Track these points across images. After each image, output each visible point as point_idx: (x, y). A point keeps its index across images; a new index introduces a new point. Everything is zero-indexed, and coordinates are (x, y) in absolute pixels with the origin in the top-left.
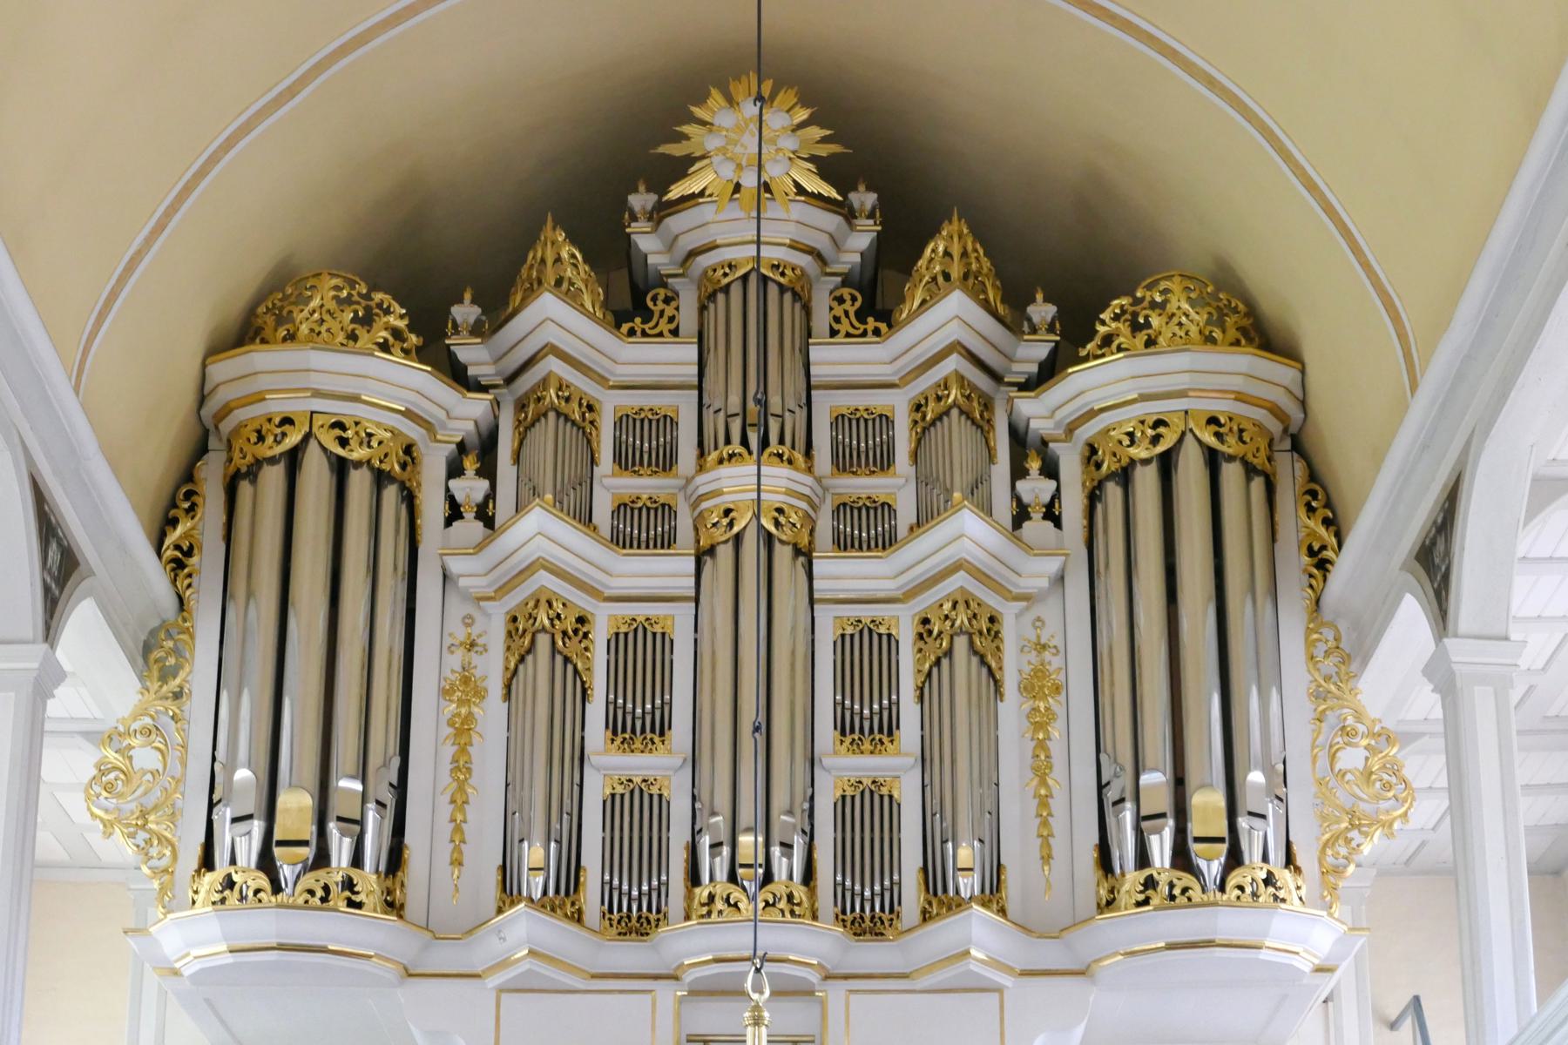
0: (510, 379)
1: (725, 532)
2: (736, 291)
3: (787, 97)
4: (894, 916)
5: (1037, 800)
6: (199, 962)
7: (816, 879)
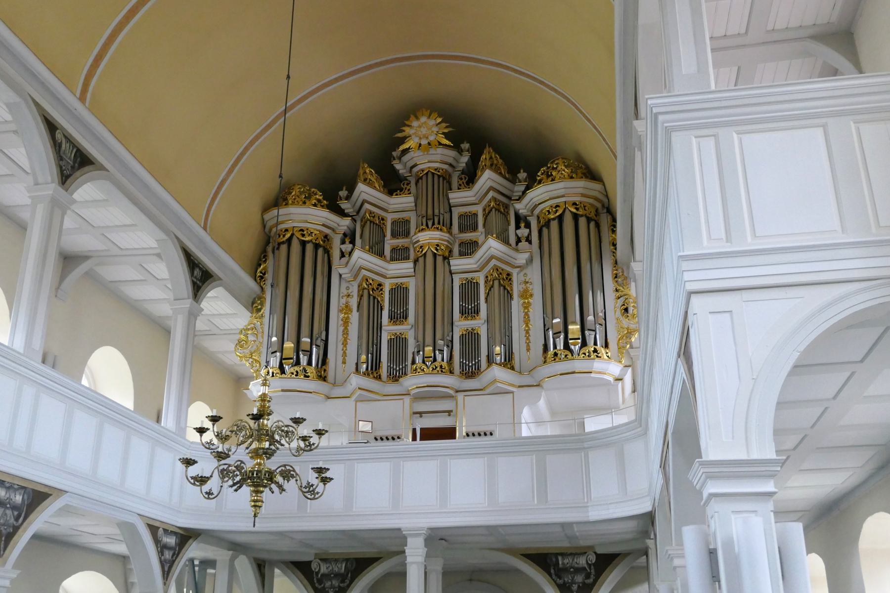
0: (358, 212)
2: (424, 178)
3: (435, 115)
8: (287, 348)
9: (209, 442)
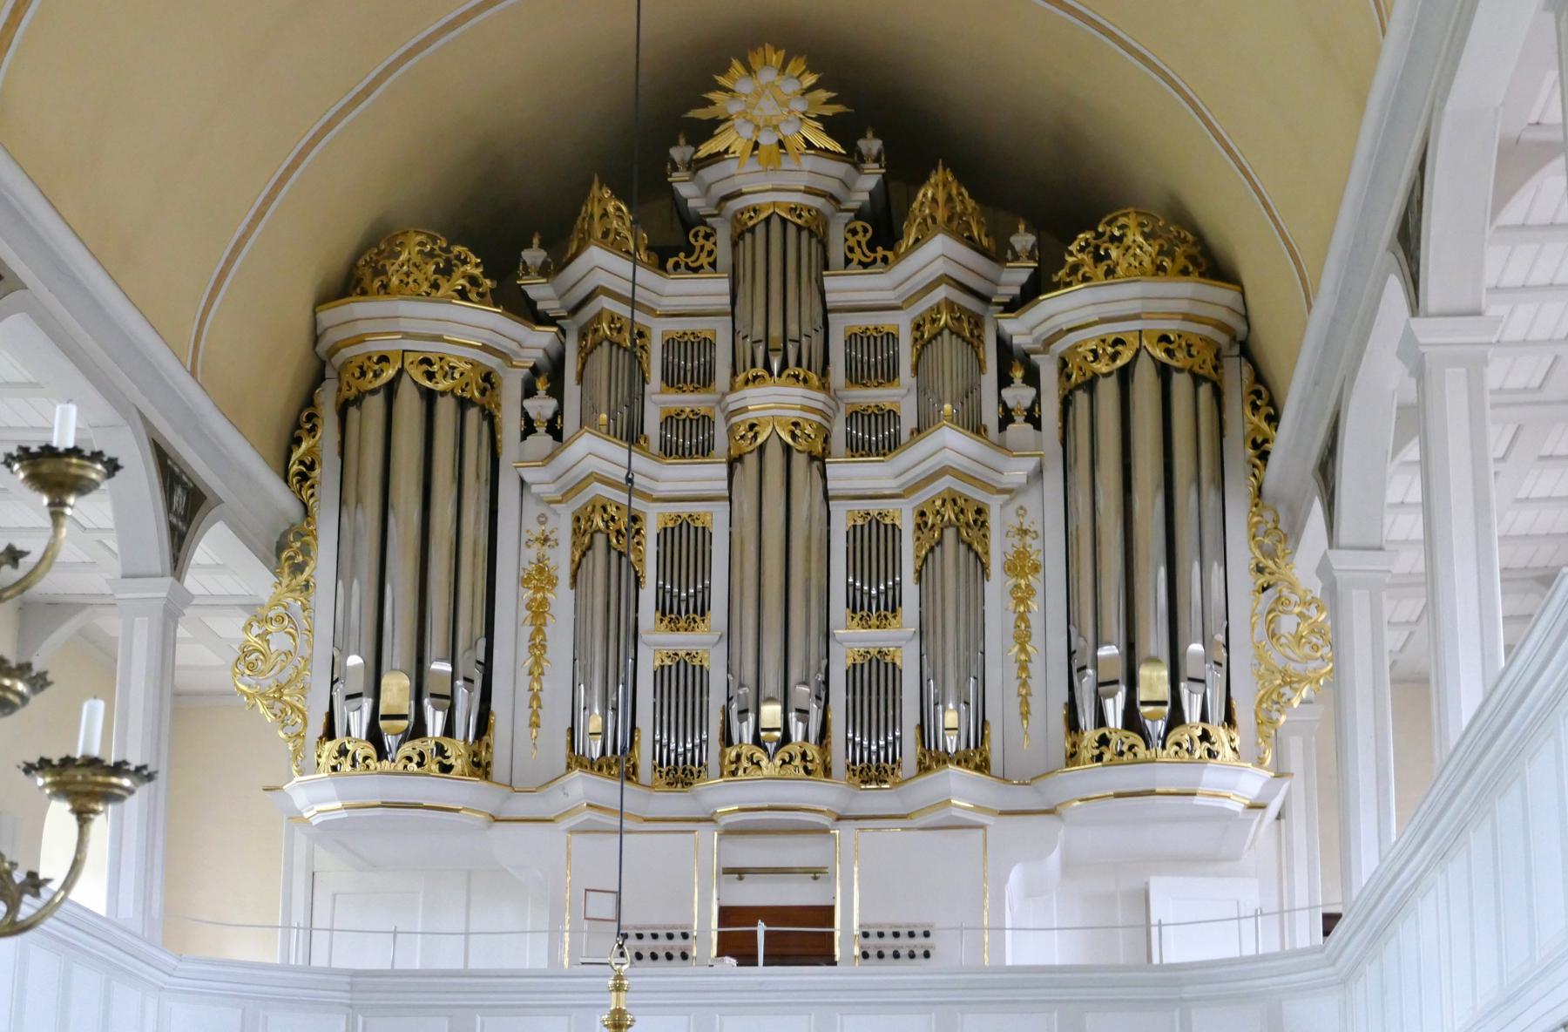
0: (575, 310)
1: (751, 444)
2: (760, 231)
3: (798, 65)
4: (895, 766)
5: (1017, 665)
6: (323, 816)
7: (830, 737)
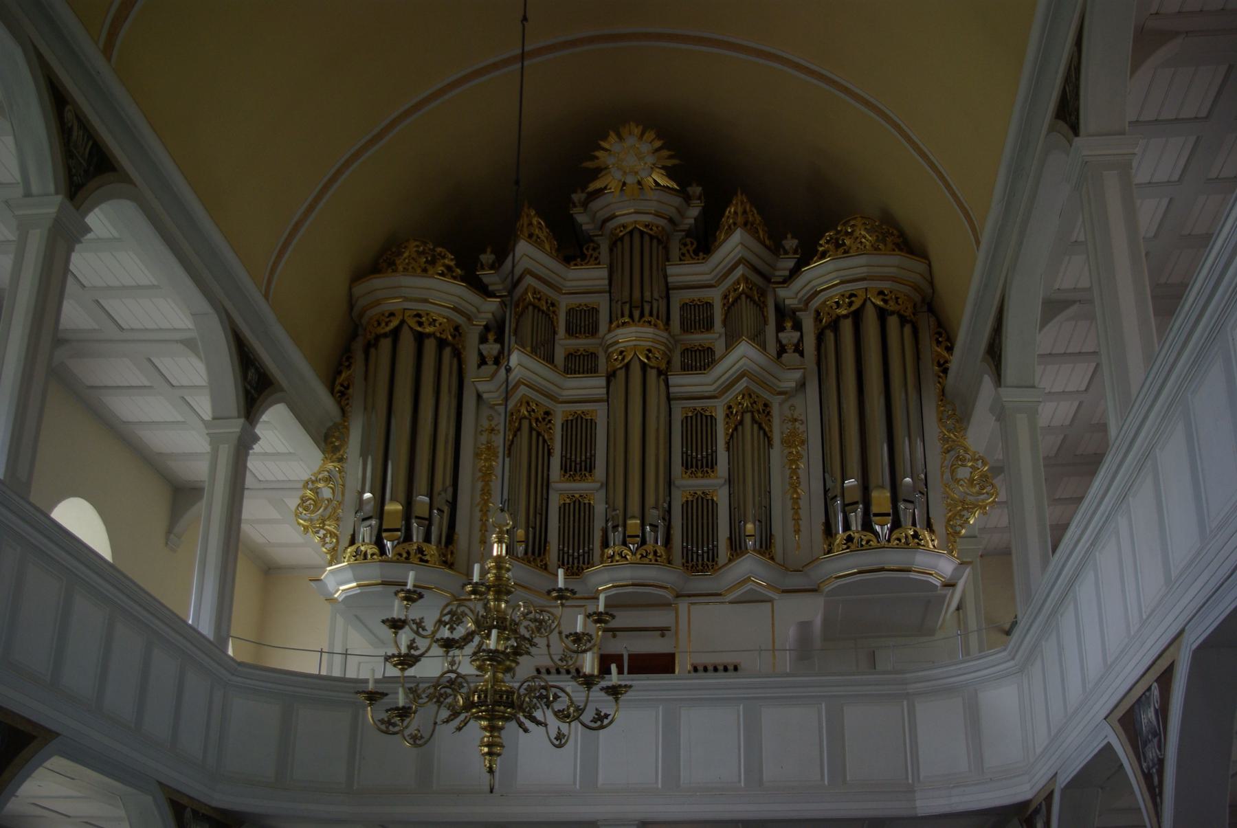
2: (627, 239)
3: (650, 135)
8: (390, 513)
9: (418, 621)
